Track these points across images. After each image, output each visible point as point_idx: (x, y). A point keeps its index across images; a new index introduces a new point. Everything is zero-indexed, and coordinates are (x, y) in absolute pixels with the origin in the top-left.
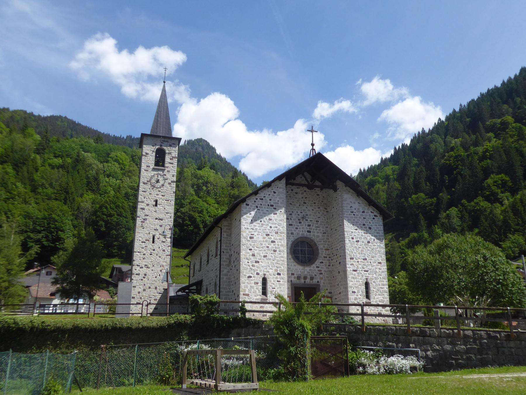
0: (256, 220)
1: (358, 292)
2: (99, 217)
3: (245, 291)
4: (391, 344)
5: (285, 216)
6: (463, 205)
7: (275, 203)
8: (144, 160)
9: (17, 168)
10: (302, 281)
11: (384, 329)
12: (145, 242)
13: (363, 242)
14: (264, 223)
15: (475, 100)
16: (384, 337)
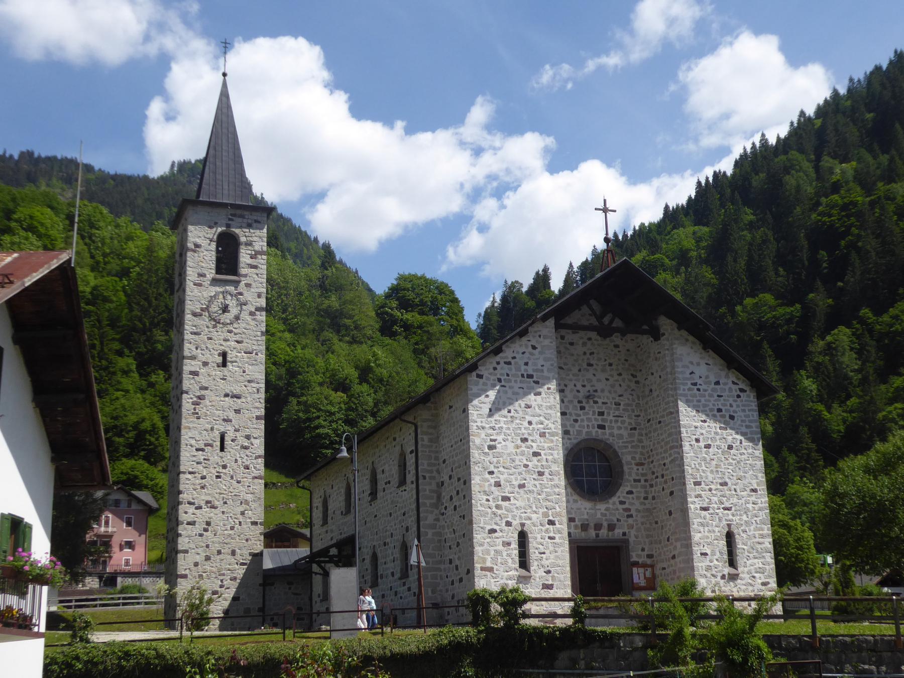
0: (500, 410)
1: (713, 553)
3: (484, 561)
4: (866, 667)
5: (558, 398)
6: (862, 321)
7: (536, 370)
10: (592, 533)
11: (853, 642)
12: (203, 450)
13: (719, 447)
14: (516, 415)
15: (885, 67)
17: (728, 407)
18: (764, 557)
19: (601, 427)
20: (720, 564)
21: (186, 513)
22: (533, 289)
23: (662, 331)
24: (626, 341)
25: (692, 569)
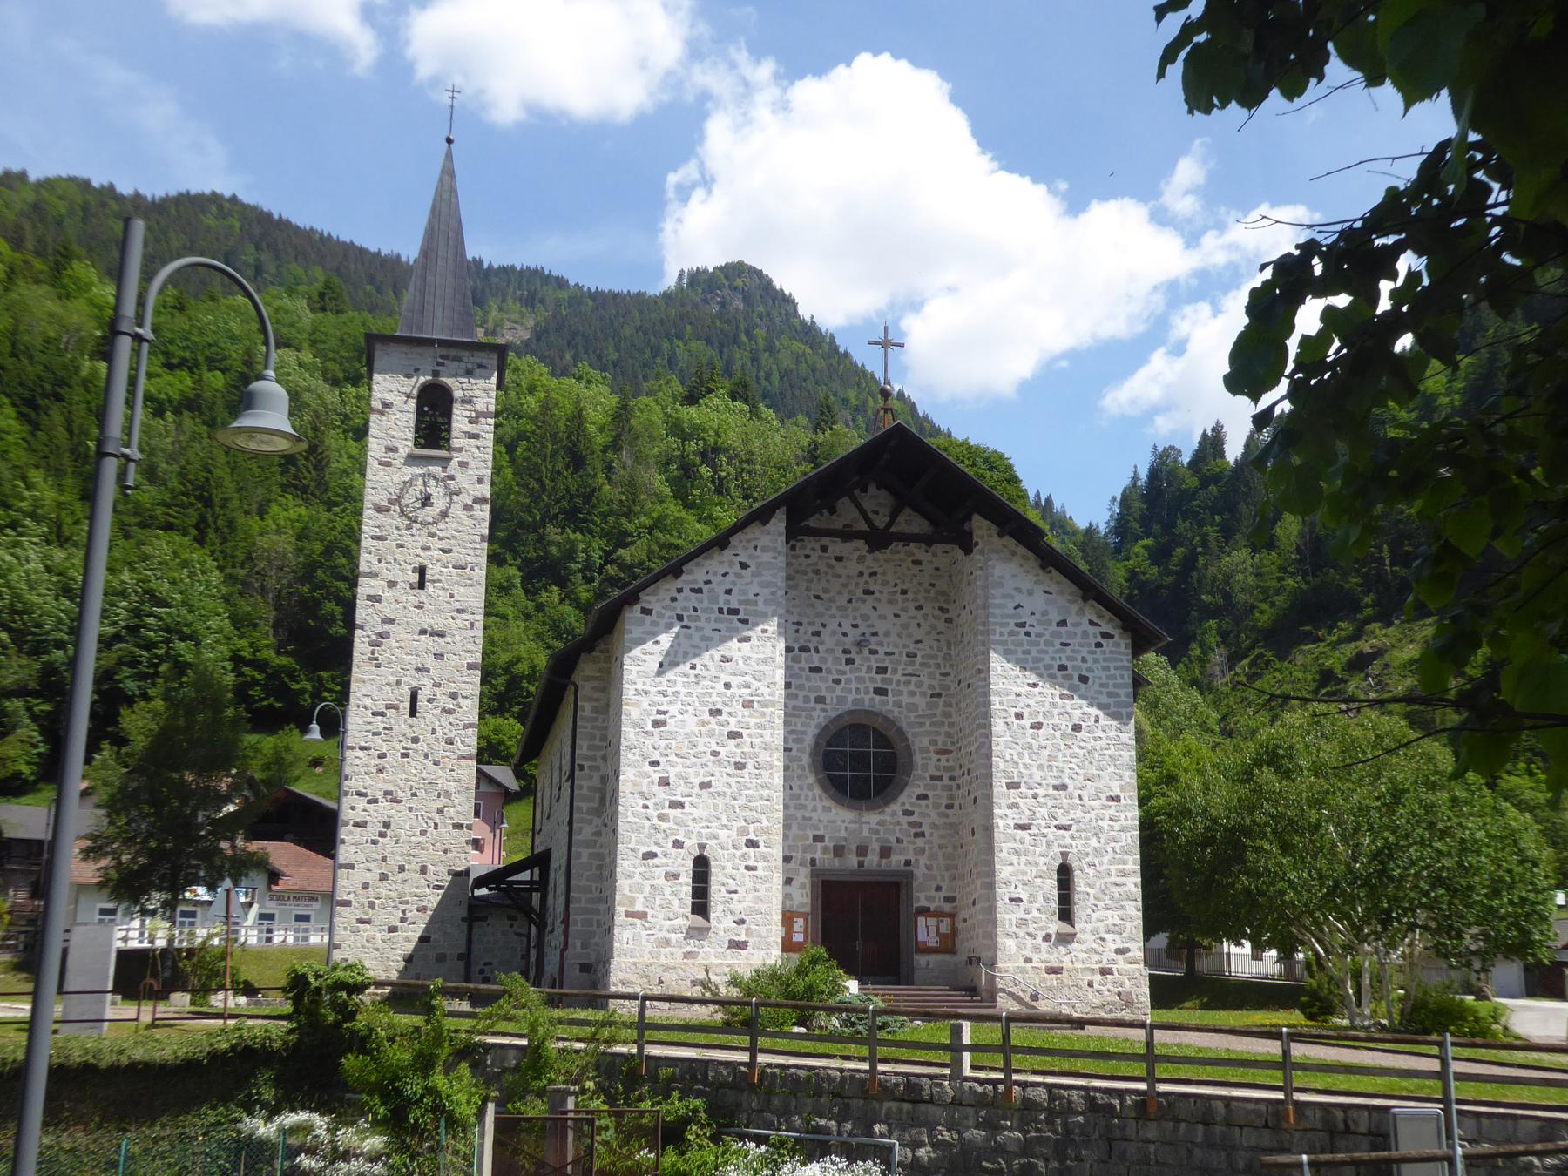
0: (677, 664)
1: (1032, 899)
2: (322, 586)
3: (632, 901)
4: (823, 1122)
7: (747, 602)
8: (376, 426)
9: (33, 414)
10: (852, 861)
11: (809, 1078)
12: (383, 714)
13: (1056, 728)
14: (705, 673)
16: (809, 1101)
17: (1079, 663)
18: (1123, 907)
19: (881, 692)
20: (1044, 917)
21: (353, 808)
22: (1199, 457)
23: (975, 539)
24: (935, 555)
25: (993, 922)
